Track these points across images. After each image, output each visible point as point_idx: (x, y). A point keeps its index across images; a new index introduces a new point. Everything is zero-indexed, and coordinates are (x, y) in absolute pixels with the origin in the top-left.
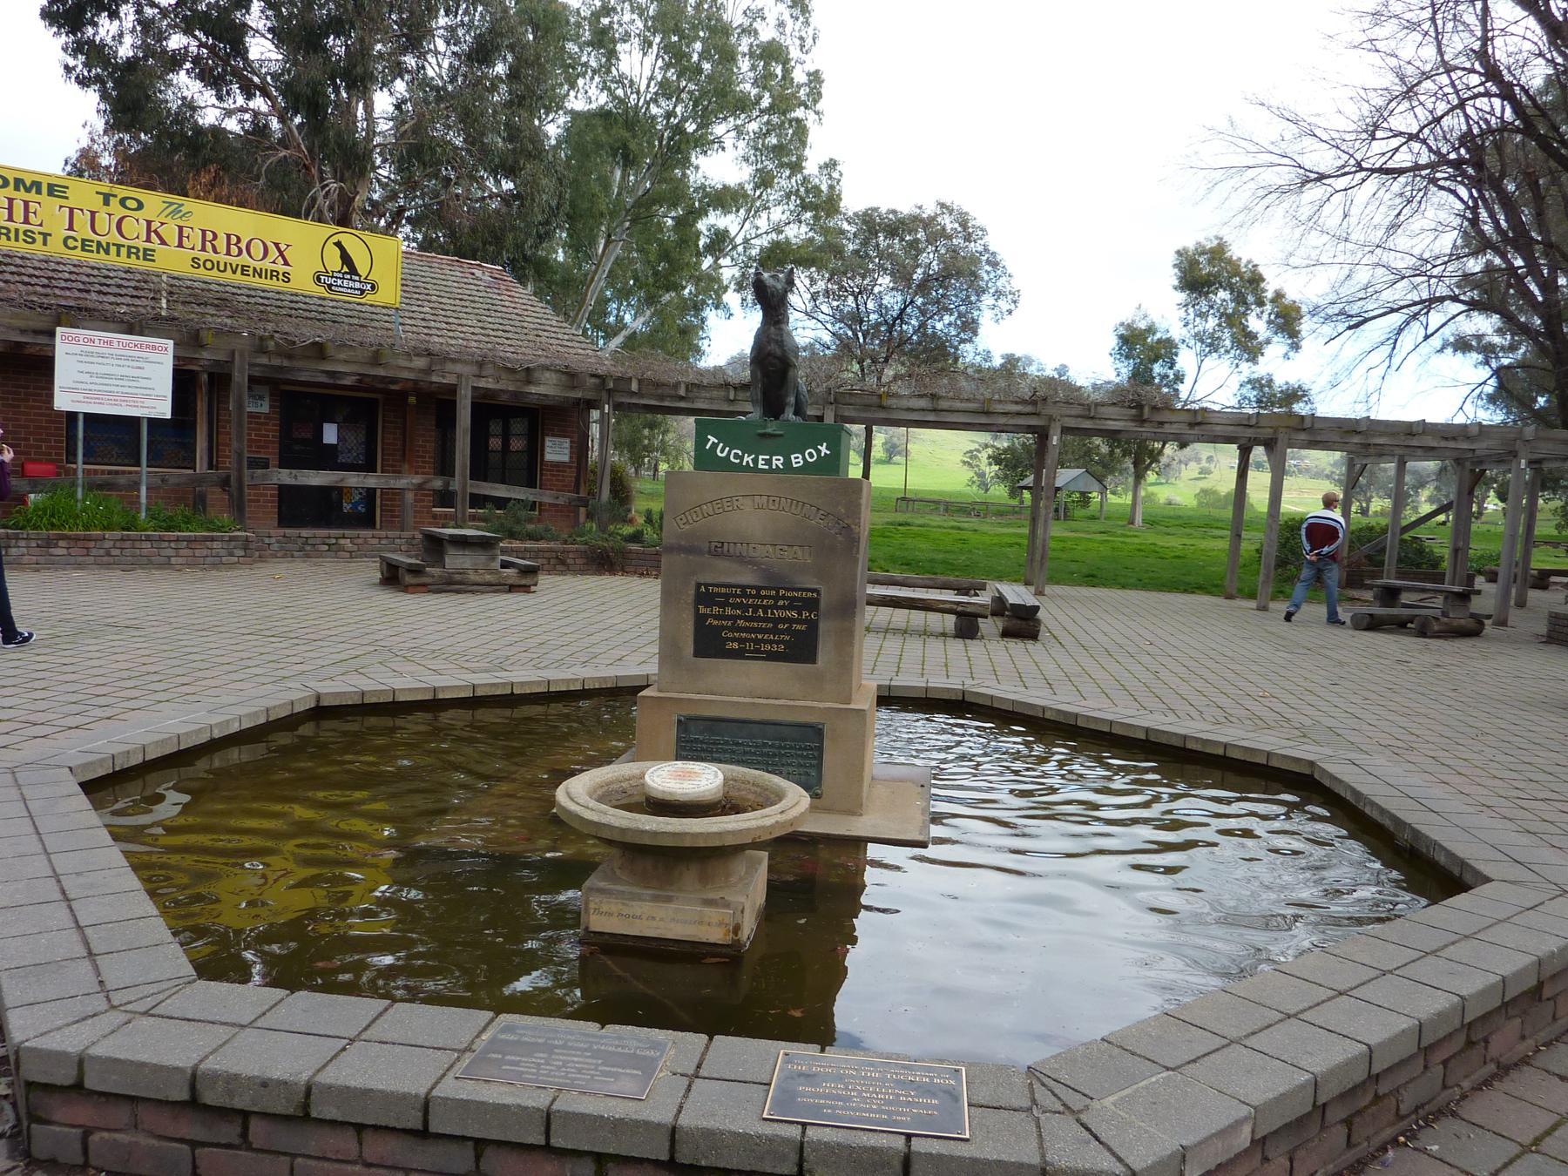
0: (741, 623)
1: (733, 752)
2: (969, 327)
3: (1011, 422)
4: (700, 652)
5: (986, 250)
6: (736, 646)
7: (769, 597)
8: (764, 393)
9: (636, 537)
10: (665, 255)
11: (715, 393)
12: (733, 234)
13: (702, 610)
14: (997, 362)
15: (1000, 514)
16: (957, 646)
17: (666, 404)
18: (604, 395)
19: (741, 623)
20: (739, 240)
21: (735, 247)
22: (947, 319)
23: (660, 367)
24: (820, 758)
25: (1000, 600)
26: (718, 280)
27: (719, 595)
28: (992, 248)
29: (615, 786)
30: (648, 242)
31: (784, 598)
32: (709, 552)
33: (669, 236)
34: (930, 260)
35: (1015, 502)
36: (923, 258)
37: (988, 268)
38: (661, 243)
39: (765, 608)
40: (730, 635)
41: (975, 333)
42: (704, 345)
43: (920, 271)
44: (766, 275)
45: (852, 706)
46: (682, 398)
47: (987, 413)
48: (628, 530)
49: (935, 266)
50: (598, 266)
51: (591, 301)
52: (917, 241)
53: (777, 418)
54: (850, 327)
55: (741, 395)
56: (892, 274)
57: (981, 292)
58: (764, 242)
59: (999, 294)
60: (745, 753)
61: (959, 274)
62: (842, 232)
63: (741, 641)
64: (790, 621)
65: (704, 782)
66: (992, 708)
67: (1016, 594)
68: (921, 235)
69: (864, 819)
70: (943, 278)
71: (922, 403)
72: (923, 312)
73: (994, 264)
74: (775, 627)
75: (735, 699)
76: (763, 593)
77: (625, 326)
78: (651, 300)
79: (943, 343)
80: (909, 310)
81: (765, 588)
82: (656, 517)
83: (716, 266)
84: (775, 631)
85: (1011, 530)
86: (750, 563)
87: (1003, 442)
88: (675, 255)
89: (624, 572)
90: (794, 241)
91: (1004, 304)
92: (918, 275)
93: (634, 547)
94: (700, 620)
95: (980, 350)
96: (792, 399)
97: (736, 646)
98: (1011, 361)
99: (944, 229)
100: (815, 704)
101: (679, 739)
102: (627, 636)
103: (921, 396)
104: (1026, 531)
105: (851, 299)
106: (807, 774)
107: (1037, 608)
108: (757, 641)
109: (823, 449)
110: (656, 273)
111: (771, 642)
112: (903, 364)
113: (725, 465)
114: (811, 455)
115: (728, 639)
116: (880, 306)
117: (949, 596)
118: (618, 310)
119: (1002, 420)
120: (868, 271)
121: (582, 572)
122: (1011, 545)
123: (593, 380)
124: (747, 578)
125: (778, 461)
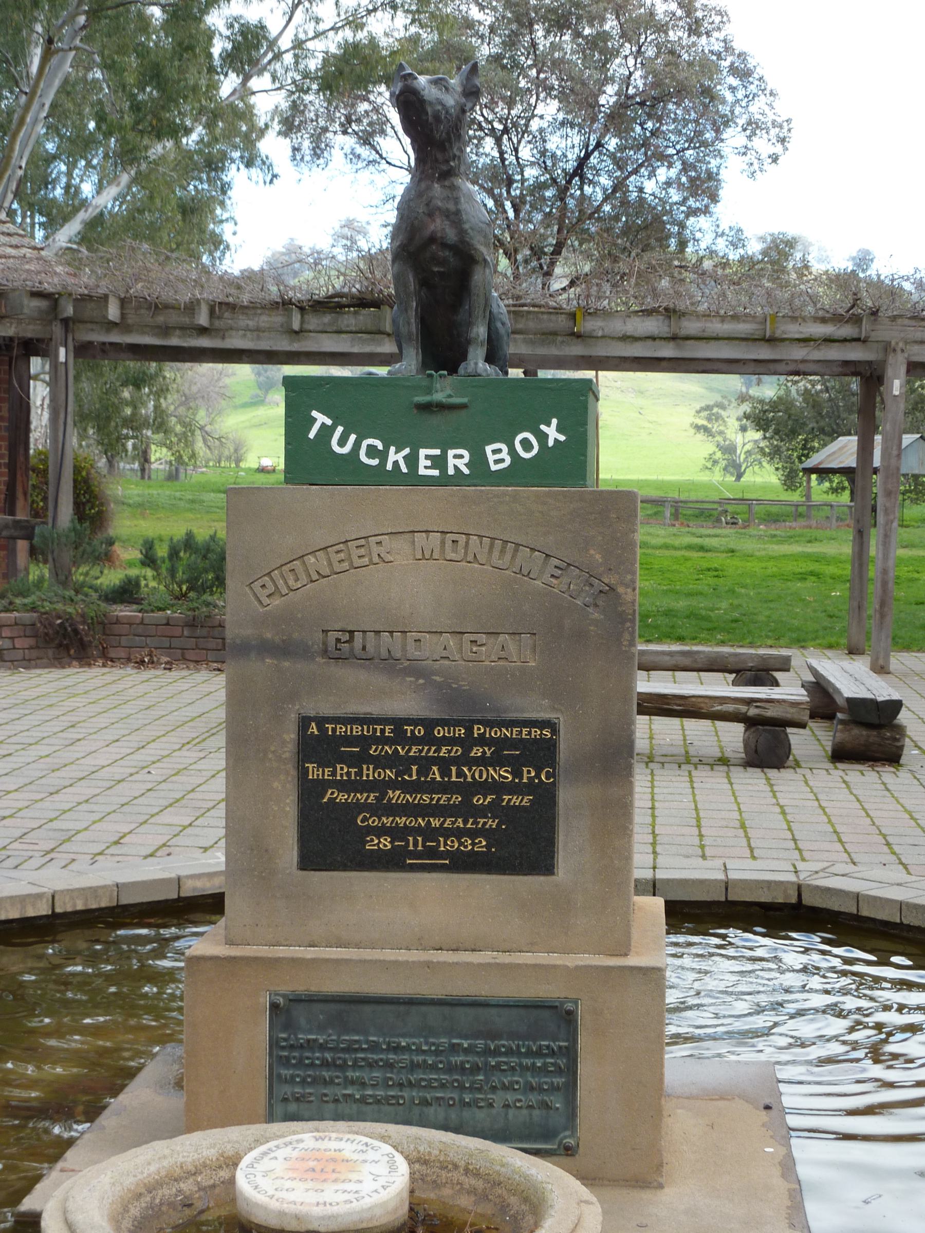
0: (395, 796)
1: (389, 1066)
2: (703, 187)
3: (817, 355)
4: (310, 860)
5: (728, 49)
6: (386, 843)
7: (452, 741)
8: (424, 321)
9: (127, 593)
10: (154, 74)
11: (264, 320)
12: (273, 31)
13: (314, 772)
14: (754, 248)
15: (773, 519)
16: (752, 782)
17: (174, 341)
18: (57, 330)
19: (395, 796)
20: (285, 43)
21: (278, 56)
22: (663, 173)
23: (149, 273)
24: (571, 1071)
25: (820, 689)
26: (247, 114)
27: (348, 740)
28: (738, 46)
29: (166, 1192)
30: (122, 50)
31: (482, 741)
32: (325, 652)
33: (158, 40)
34: (628, 70)
35: (795, 497)
36: (617, 67)
37: (733, 81)
38: (142, 52)
39: (445, 765)
40: (374, 822)
41: (714, 198)
42: (226, 231)
43: (611, 89)
44: (422, 80)
45: (633, 961)
46: (203, 331)
47: (772, 341)
48: (111, 578)
49: (638, 80)
50: (31, 96)
51: (21, 160)
52: (604, 36)
53: (453, 370)
54: (490, 192)
55: (313, 322)
56: (562, 97)
57: (722, 123)
58: (332, 44)
59: (753, 127)
60: (414, 1067)
61: (681, 92)
62: (469, 24)
63: (395, 833)
64: (498, 788)
65: (368, 1186)
66: (857, 917)
67: (852, 678)
68: (611, 24)
69: (669, 1195)
70: (653, 102)
71: (652, 326)
72: (620, 164)
73: (743, 73)
74: (467, 801)
75: (389, 955)
76: (439, 732)
77: (84, 203)
78: (128, 155)
79: (657, 218)
80: (593, 160)
81: (444, 723)
82: (162, 551)
83: (244, 92)
84: (467, 810)
85: (796, 549)
86: (407, 672)
87: (769, 389)
88: (171, 73)
89: (107, 659)
90: (384, 42)
91: (763, 145)
92: (608, 97)
93: (124, 611)
94: (309, 792)
95: (724, 226)
96: (481, 331)
97: (386, 843)
98: (780, 250)
99: (652, 14)
100: (555, 959)
101: (274, 1044)
102: (126, 791)
103: (648, 313)
104: (847, 549)
105: (489, 142)
106: (546, 1106)
107: (896, 706)
108: (429, 833)
109: (552, 432)
110: (136, 107)
111: (459, 834)
112: (588, 256)
113: (349, 471)
114: (526, 445)
115: (370, 830)
116: (543, 153)
117: (718, 686)
118: (69, 174)
119: (798, 353)
120: (517, 91)
121: (28, 663)
122: (803, 577)
123: (36, 303)
124: (405, 702)
125: (458, 460)
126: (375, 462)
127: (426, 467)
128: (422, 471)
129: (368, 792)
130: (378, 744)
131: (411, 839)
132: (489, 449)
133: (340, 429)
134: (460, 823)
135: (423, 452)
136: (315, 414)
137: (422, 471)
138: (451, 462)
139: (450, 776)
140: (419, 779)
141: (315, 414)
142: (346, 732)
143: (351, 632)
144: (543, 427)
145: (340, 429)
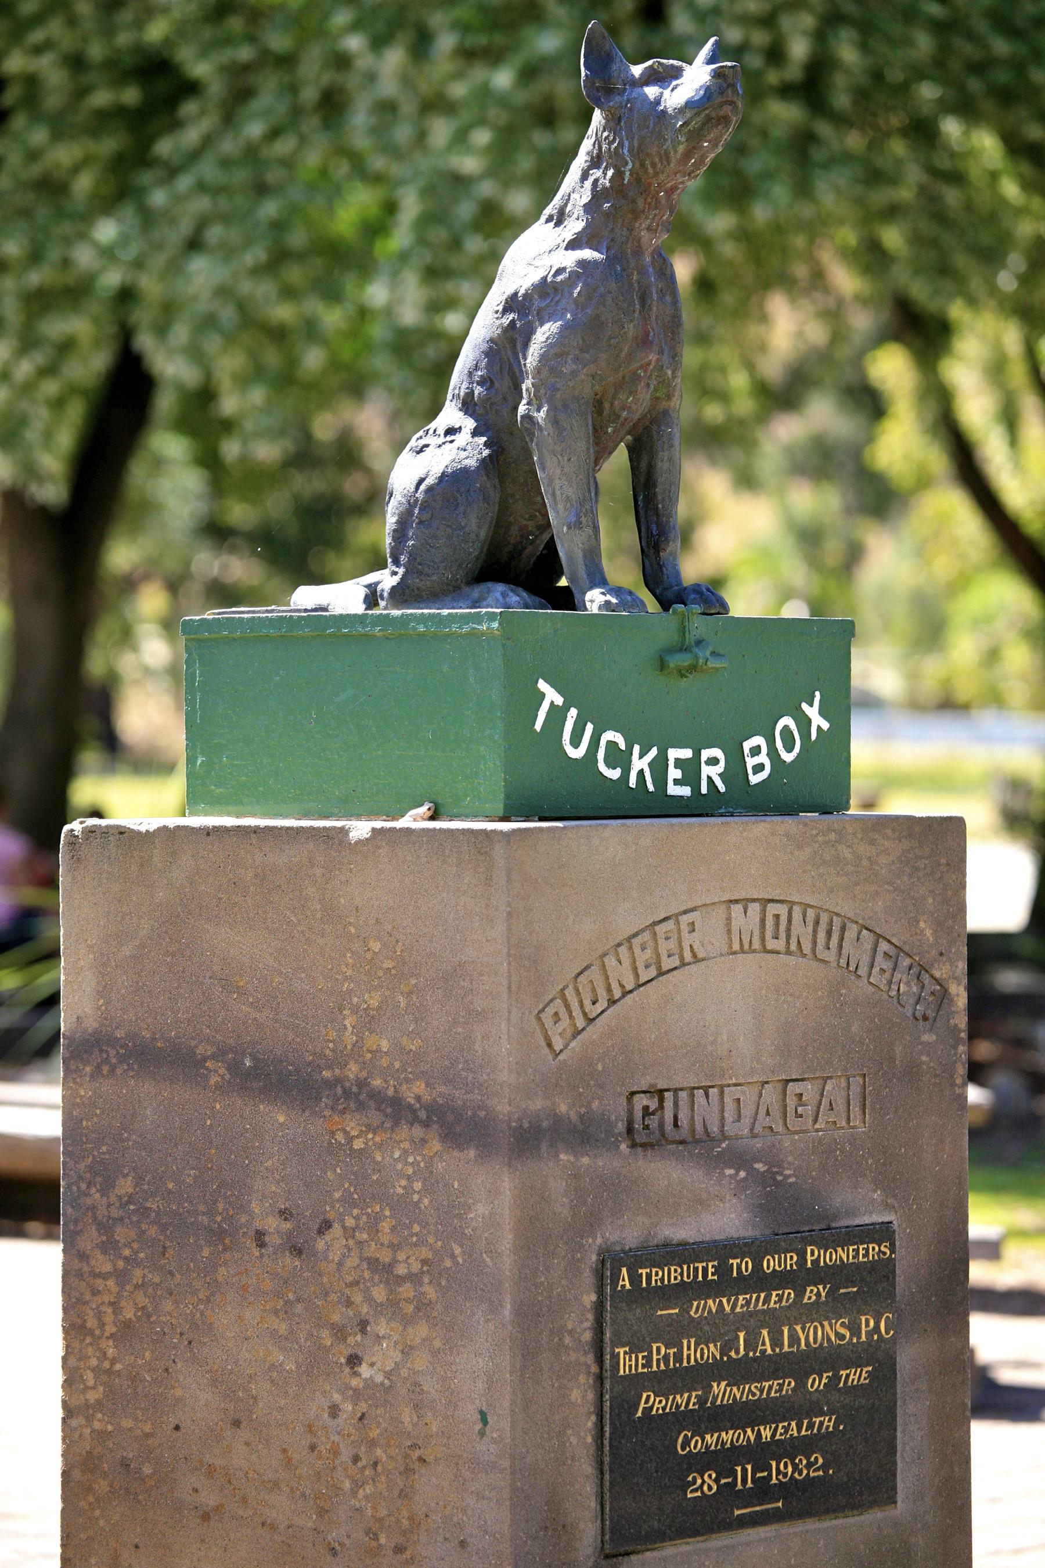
31: (817, 1274)
94: (615, 1402)
108: (760, 1454)
126: (615, 774)
127: (676, 782)
129: (689, 1390)
130: (757, 1312)
131: (739, 1469)
132: (747, 745)
133: (573, 712)
134: (766, 1433)
135: (673, 754)
136: (542, 685)
137: (673, 790)
138: (706, 771)
139: (782, 1346)
140: (747, 1354)
141: (542, 685)
142: (662, 1280)
143: (661, 1092)
144: (805, 706)
145: (573, 712)
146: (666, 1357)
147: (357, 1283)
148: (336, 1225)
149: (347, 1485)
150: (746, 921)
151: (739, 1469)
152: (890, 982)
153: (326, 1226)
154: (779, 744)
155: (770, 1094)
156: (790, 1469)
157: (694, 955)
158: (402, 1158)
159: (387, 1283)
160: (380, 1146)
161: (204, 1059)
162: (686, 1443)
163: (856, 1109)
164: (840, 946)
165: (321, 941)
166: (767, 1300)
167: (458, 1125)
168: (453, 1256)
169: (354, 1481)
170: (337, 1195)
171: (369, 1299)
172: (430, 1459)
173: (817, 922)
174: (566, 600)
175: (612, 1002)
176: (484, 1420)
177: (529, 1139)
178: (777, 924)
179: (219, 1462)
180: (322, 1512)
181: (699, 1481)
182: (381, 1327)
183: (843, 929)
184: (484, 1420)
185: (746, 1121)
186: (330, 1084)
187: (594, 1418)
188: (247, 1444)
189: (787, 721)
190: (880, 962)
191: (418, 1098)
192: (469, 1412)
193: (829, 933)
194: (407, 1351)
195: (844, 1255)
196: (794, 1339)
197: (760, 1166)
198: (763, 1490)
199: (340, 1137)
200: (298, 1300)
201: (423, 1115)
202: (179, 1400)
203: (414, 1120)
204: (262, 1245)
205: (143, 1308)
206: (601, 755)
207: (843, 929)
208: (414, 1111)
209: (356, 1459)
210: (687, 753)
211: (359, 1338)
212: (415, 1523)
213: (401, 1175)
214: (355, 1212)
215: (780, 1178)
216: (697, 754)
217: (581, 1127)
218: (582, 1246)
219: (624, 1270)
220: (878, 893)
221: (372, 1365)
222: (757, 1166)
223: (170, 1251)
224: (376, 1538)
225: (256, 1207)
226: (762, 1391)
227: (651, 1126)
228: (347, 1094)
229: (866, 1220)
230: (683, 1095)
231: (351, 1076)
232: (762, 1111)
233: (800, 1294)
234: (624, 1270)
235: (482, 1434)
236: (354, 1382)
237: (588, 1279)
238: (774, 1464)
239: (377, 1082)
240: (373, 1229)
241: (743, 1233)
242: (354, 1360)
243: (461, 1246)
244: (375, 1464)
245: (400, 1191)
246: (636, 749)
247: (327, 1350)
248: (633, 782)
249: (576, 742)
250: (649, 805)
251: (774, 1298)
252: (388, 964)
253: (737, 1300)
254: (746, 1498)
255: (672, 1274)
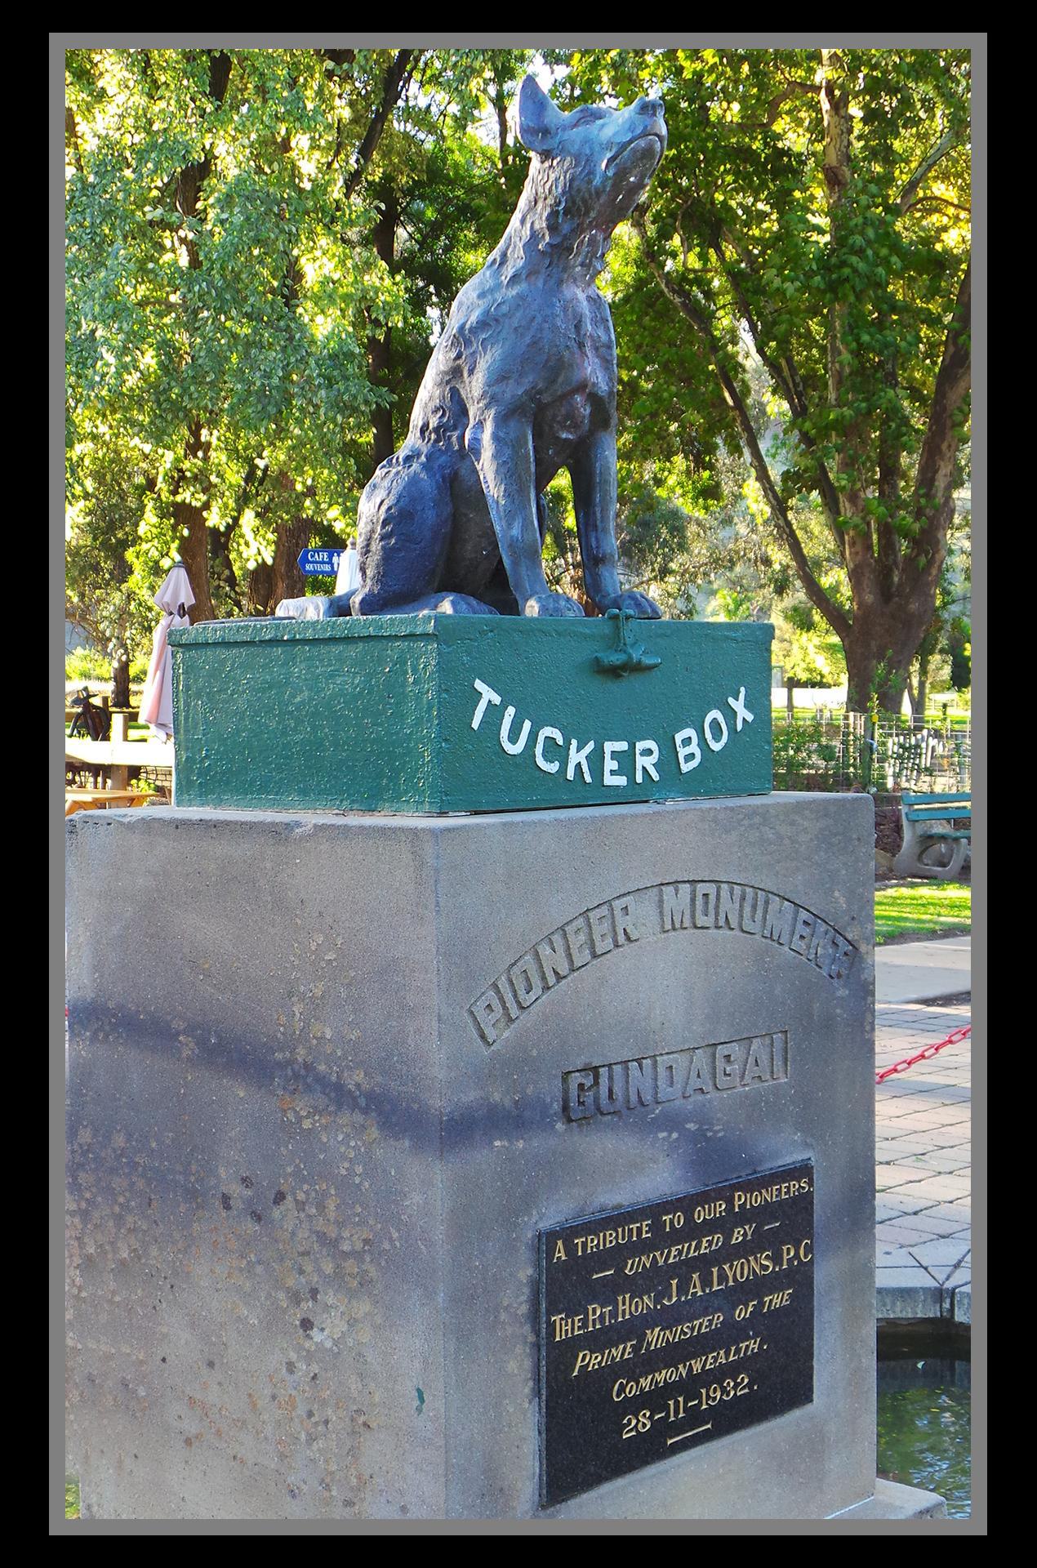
31: (744, 1216)
94: (553, 1361)
108: (690, 1386)
126: (553, 768)
127: (612, 772)
128: (609, 780)
129: (624, 1342)
130: (687, 1260)
131: (671, 1403)
132: (679, 738)
133: (511, 710)
135: (609, 747)
136: (479, 685)
137: (609, 780)
138: (641, 761)
141: (479, 685)
143: (595, 1070)
144: (731, 700)
145: (511, 710)
146: (602, 1316)
147: (308, 1253)
148: (289, 1198)
149: (303, 1436)
150: (677, 901)
151: (671, 1403)
152: (809, 948)
153: (280, 1197)
154: (708, 735)
155: (701, 1059)
156: (718, 1394)
157: (628, 939)
158: (346, 1140)
159: (334, 1257)
160: (325, 1128)
161: (178, 1034)
162: (622, 1388)
163: (778, 1062)
164: (765, 919)
165: (272, 931)
166: (698, 1247)
167: (394, 1113)
168: (391, 1240)
169: (309, 1434)
170: (289, 1170)
171: (319, 1270)
172: (373, 1425)
173: (743, 898)
174: (512, 607)
175: (546, 988)
176: (422, 1399)
177: (460, 1130)
178: (706, 903)
179: (198, 1396)
180: (282, 1457)
181: (634, 1422)
182: (329, 1297)
183: (767, 902)
184: (422, 1399)
185: (678, 1086)
186: (282, 1066)
187: (531, 1383)
188: (220, 1384)
189: (714, 714)
190: (801, 929)
191: (358, 1085)
192: (408, 1388)
193: (754, 907)
194: (352, 1323)
195: (770, 1195)
196: (723, 1278)
197: (691, 1126)
198: (695, 1417)
199: (291, 1116)
200: (259, 1262)
201: (362, 1102)
202: (165, 1336)
203: (354, 1106)
204: (228, 1207)
205: (135, 1250)
206: (539, 750)
207: (767, 902)
208: (355, 1099)
209: (310, 1414)
210: (623, 746)
211: (310, 1304)
212: (363, 1483)
213: (344, 1157)
214: (306, 1187)
215: (709, 1134)
216: (632, 746)
217: (515, 1112)
218: (516, 1225)
219: (560, 1243)
220: (798, 869)
221: (322, 1330)
222: (688, 1126)
223: (154, 1204)
224: (328, 1488)
225: (222, 1172)
226: (693, 1329)
227: (588, 1100)
228: (296, 1076)
229: (788, 1160)
230: (617, 1069)
231: (300, 1060)
232: (694, 1074)
233: (728, 1236)
234: (560, 1243)
235: (419, 1410)
236: (307, 1345)
237: (524, 1254)
238: (703, 1391)
239: (322, 1068)
240: (321, 1207)
241: (674, 1189)
242: (307, 1324)
243: (398, 1231)
244: (326, 1422)
245: (344, 1172)
246: (574, 742)
247: (285, 1311)
248: (570, 775)
249: (513, 739)
250: (587, 793)
251: (705, 1244)
252: (330, 956)
253: (669, 1252)
254: (678, 1427)
255: (610, 1239)
